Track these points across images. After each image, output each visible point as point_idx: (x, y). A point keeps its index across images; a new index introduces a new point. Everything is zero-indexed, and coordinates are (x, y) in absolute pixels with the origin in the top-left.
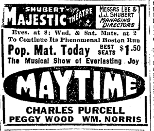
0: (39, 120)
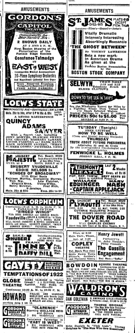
0: (92, 244)
